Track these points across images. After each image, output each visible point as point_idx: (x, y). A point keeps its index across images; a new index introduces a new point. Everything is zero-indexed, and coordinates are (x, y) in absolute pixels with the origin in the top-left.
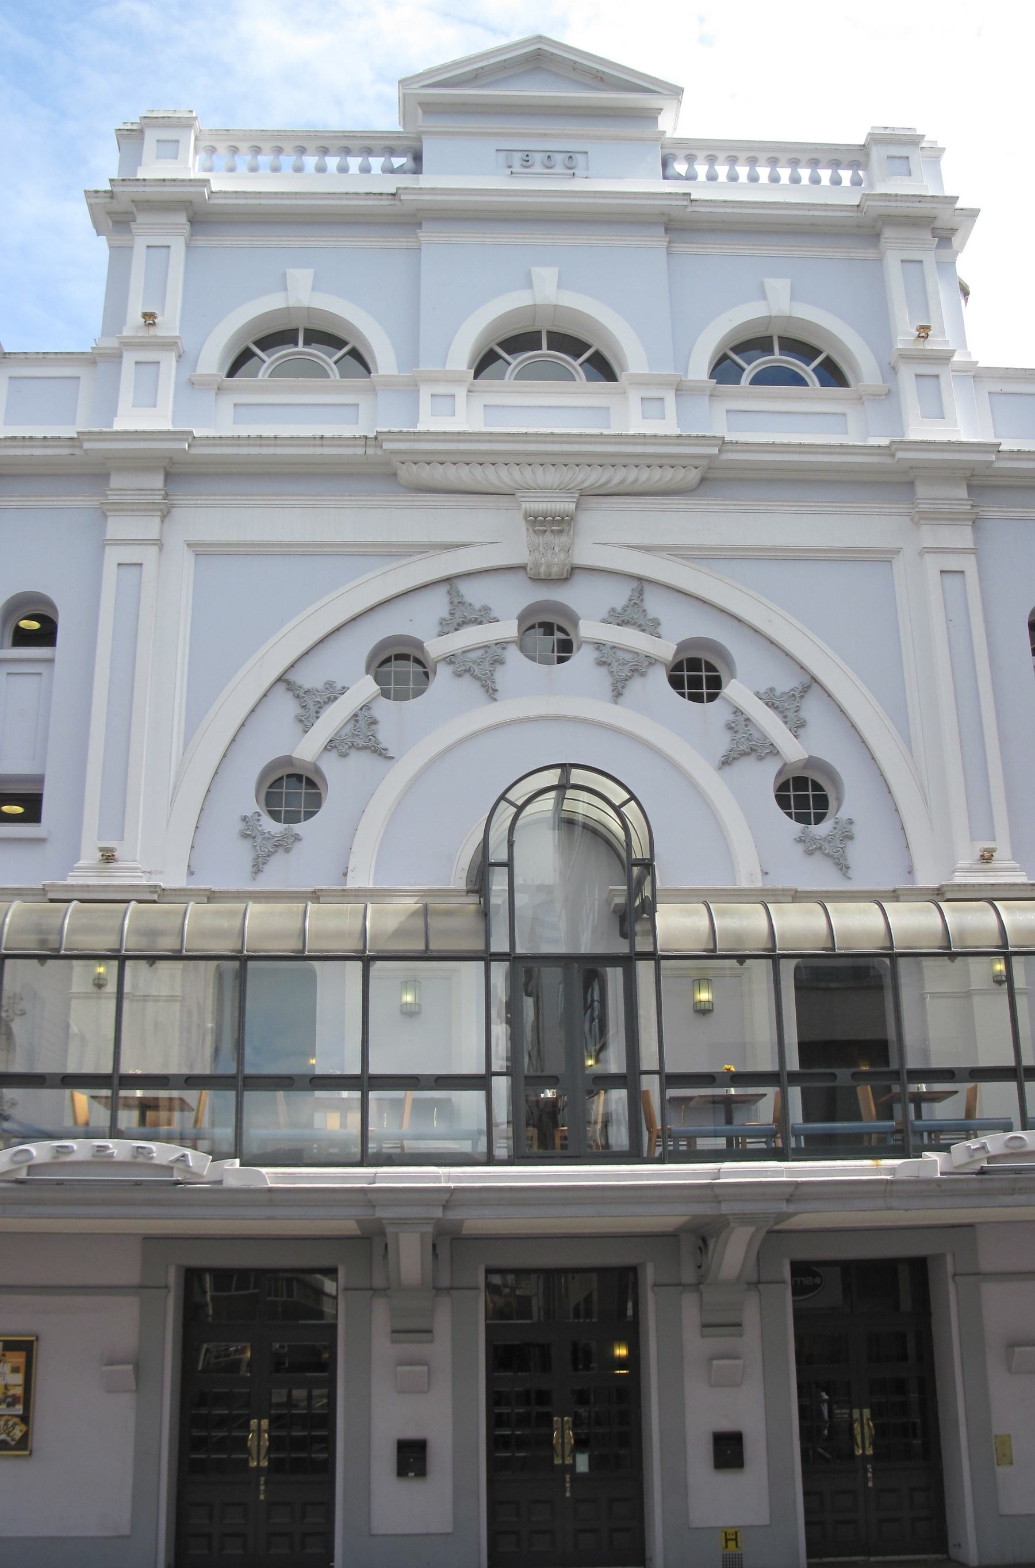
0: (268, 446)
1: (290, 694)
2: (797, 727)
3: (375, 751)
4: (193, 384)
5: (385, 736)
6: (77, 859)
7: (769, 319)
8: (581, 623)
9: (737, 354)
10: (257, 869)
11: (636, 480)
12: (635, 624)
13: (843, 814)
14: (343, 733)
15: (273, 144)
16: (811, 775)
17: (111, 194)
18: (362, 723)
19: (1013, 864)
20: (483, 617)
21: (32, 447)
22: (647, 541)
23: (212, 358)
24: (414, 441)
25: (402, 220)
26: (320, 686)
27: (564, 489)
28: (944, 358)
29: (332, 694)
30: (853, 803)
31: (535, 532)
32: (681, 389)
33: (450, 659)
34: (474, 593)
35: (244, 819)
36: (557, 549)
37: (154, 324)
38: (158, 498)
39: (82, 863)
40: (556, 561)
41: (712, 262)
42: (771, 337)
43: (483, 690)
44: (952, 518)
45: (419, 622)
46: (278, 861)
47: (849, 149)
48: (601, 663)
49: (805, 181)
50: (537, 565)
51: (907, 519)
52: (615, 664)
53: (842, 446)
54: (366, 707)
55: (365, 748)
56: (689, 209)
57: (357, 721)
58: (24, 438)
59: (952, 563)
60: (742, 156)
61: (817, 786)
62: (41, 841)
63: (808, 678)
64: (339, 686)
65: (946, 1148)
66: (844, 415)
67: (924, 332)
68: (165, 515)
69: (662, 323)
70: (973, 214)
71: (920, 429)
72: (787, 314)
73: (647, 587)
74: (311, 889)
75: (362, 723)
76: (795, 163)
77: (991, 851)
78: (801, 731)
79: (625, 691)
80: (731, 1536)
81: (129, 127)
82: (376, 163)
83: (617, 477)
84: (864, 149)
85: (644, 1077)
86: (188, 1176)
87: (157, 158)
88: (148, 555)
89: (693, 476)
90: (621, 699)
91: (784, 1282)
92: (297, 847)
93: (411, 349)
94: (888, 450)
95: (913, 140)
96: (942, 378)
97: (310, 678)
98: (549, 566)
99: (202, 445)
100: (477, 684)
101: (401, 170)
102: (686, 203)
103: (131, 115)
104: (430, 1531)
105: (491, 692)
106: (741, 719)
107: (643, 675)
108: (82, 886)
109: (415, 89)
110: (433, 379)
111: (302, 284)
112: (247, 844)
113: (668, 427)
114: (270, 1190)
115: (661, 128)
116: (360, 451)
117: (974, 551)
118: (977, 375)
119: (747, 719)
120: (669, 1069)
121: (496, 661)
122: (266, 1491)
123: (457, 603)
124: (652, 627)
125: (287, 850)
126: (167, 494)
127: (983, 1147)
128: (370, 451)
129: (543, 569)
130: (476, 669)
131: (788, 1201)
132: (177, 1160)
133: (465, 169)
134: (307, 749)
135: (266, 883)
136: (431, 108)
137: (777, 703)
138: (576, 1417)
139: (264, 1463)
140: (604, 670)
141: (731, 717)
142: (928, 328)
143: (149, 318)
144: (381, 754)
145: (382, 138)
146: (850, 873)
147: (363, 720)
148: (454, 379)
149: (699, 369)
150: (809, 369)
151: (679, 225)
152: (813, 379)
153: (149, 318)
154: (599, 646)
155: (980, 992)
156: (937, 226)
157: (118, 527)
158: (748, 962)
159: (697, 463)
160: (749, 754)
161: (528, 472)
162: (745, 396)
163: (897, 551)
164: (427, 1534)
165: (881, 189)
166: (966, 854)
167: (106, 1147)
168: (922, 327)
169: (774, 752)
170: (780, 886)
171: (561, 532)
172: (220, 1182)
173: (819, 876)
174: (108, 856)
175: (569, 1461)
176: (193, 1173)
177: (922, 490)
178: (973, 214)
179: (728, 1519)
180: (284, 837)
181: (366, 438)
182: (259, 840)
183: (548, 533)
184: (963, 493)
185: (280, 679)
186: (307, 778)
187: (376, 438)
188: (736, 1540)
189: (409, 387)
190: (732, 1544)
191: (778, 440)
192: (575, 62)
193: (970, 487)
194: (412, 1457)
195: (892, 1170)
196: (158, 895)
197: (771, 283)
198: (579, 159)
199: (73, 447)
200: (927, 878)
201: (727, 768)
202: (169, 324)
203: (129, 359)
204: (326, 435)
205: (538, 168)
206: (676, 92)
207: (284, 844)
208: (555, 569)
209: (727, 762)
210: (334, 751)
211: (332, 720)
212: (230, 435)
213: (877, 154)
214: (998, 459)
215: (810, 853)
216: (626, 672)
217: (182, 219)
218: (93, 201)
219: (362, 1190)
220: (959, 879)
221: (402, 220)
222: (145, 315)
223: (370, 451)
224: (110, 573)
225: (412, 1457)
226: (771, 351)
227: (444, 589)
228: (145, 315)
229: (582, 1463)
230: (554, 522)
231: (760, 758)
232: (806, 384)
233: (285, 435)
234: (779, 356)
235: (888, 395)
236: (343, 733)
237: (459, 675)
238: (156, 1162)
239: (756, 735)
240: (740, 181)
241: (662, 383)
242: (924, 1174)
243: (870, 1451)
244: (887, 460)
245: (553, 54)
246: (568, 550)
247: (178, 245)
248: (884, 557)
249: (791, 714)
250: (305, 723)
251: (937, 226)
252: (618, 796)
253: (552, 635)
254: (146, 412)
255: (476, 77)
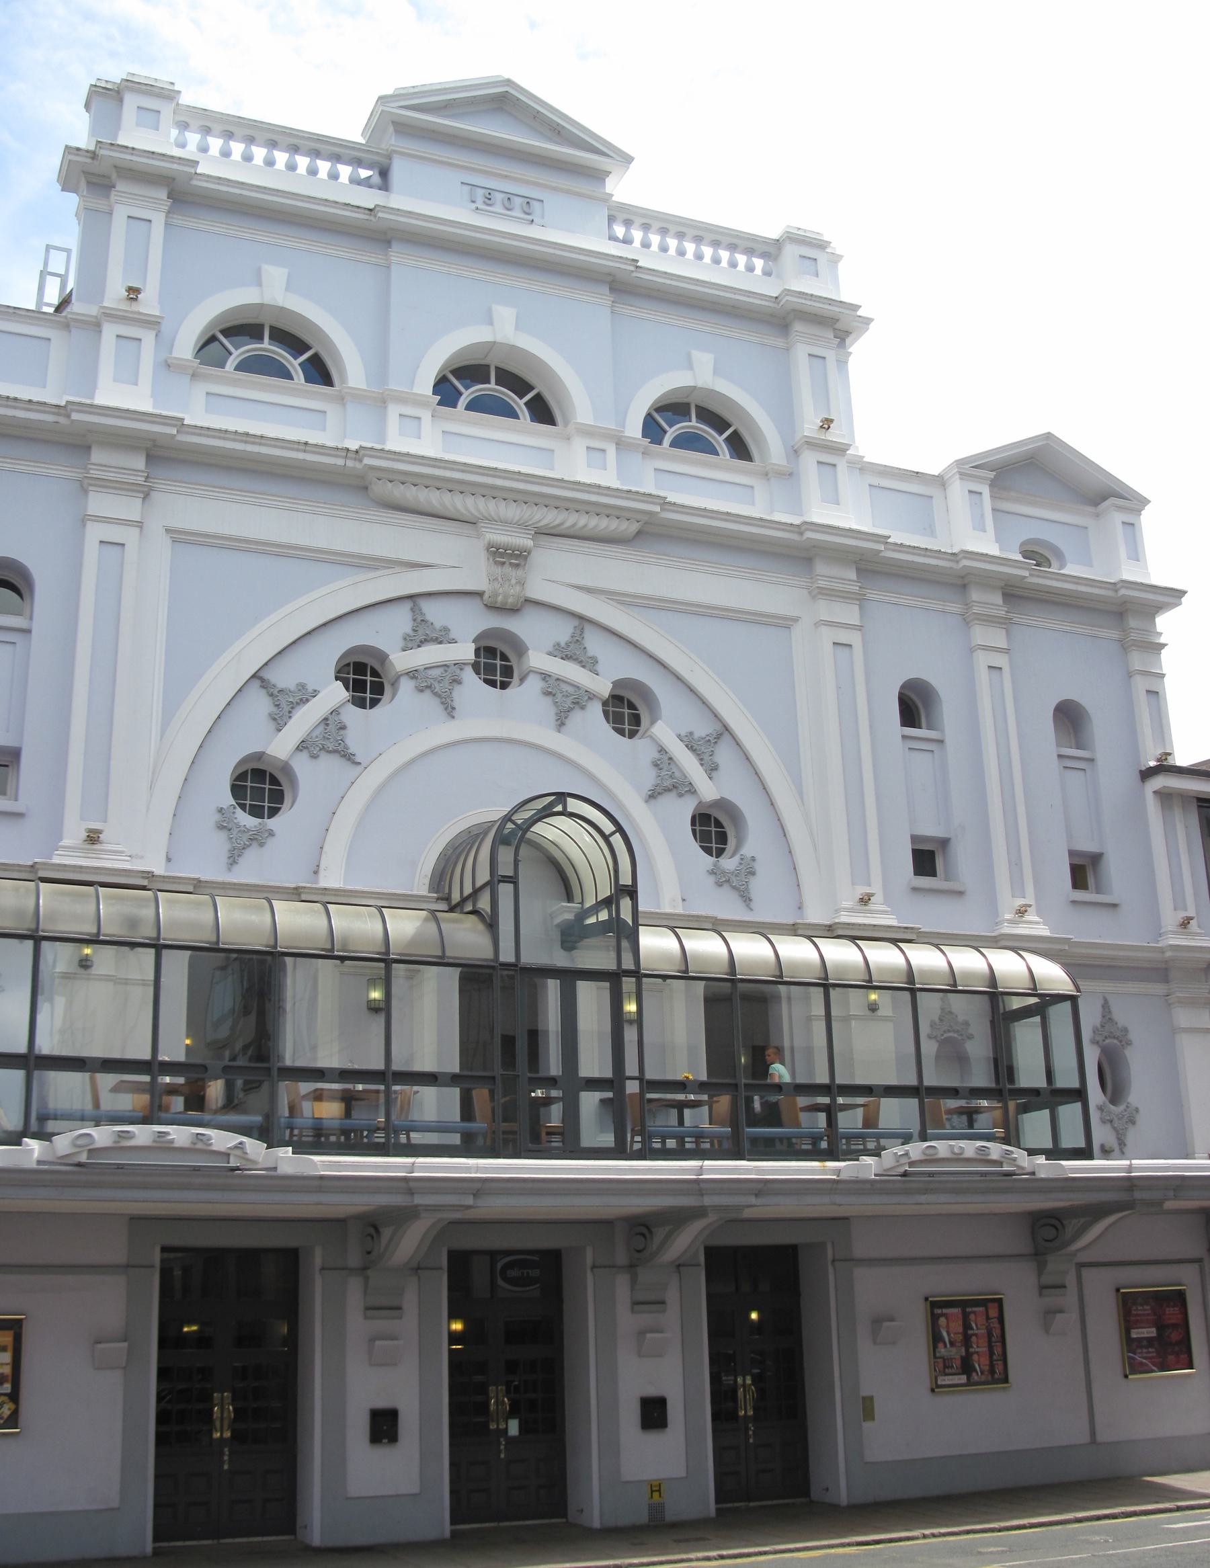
0: (253, 443)
1: (264, 691)
2: (712, 769)
3: (344, 756)
4: (169, 365)
5: (353, 742)
6: (61, 839)
7: (694, 388)
8: (530, 652)
9: (457, 378)
10: (233, 859)
11: (585, 526)
12: (576, 660)
13: (748, 850)
14: (314, 735)
15: (202, 123)
16: (716, 813)
17: (93, 155)
18: (332, 728)
19: (1036, 919)
20: (442, 637)
21: (15, 408)
22: (590, 584)
23: (185, 345)
24: (393, 460)
25: (377, 235)
26: (292, 687)
27: (522, 525)
28: (840, 450)
29: (304, 696)
30: (755, 842)
31: (496, 563)
32: (622, 444)
33: (413, 674)
34: (435, 612)
35: (221, 810)
36: (513, 581)
37: (136, 299)
38: (140, 480)
39: (66, 842)
40: (510, 593)
41: (653, 329)
42: (488, 366)
43: (442, 707)
44: (845, 596)
45: (385, 635)
46: (252, 855)
47: (765, 241)
48: (548, 693)
49: (741, 267)
50: (496, 594)
51: (806, 592)
52: (559, 696)
53: (761, 519)
54: (335, 712)
55: (335, 751)
56: (634, 274)
57: (327, 725)
58: (8, 398)
59: (844, 636)
60: (656, 225)
61: (718, 824)
62: (20, 815)
63: (719, 727)
64: (310, 688)
65: (876, 1153)
66: (752, 487)
67: (827, 424)
68: (146, 497)
69: (605, 374)
70: (868, 321)
71: (821, 514)
72: (281, 304)
73: (588, 629)
74: (293, 885)
75: (332, 728)
76: (229, 135)
77: (870, 896)
78: (714, 774)
79: (567, 721)
80: (656, 1488)
81: (103, 85)
82: (345, 171)
83: (571, 520)
84: (778, 244)
85: (628, 1082)
86: (244, 1162)
87: (138, 125)
88: (128, 536)
89: (634, 527)
90: (563, 729)
91: (699, 1265)
92: (271, 842)
93: (380, 364)
94: (799, 529)
95: (822, 245)
96: (839, 468)
97: (284, 678)
98: (506, 597)
99: (188, 433)
100: (437, 701)
101: (366, 183)
102: (632, 268)
103: (114, 73)
104: (400, 1492)
105: (450, 710)
106: (665, 758)
107: (583, 708)
108: (74, 866)
109: (392, 108)
110: (402, 399)
111: (278, 282)
112: (223, 835)
113: (609, 478)
114: (322, 1178)
115: (608, 190)
116: (340, 462)
117: (859, 628)
118: (863, 467)
119: (670, 759)
120: (649, 1075)
121: (454, 681)
122: (230, 1461)
123: (420, 621)
124: (591, 664)
125: (262, 845)
126: (147, 477)
127: (906, 1154)
128: (350, 463)
129: (500, 598)
130: (437, 685)
131: (756, 1195)
132: (236, 1147)
133: (429, 195)
134: (281, 747)
135: (244, 874)
136: (403, 128)
137: (696, 747)
138: (508, 1384)
139: (227, 1434)
140: (549, 700)
141: (656, 755)
142: (832, 421)
143: (133, 293)
144: (349, 759)
145: (354, 148)
146: (753, 905)
147: (331, 723)
148: (417, 401)
149: (634, 429)
150: (296, 363)
151: (624, 286)
152: (524, 413)
153: (133, 293)
154: (545, 676)
155: (856, 1017)
156: (835, 325)
157: (99, 503)
158: (669, 981)
159: (639, 517)
160: (670, 790)
161: (492, 504)
162: (461, 421)
163: (796, 620)
164: (397, 1496)
165: (796, 286)
166: (847, 897)
167: (167, 1133)
168: (827, 420)
169: (692, 791)
170: (704, 914)
171: (517, 565)
172: (275, 1169)
173: (726, 906)
174: (93, 838)
175: (502, 1426)
176: (248, 1160)
177: (821, 568)
178: (868, 321)
179: (651, 1473)
180: (259, 832)
181: (348, 450)
182: (235, 831)
183: (507, 565)
184: (853, 575)
185: (254, 676)
186: (271, 775)
187: (357, 452)
188: (659, 1491)
189: (380, 401)
190: (656, 1495)
191: (709, 507)
192: (538, 112)
193: (1004, 595)
194: (654, 1413)
195: (838, 1171)
196: (146, 883)
197: (696, 354)
198: (535, 204)
199: (59, 414)
200: (815, 915)
201: (653, 802)
202: (149, 304)
203: (110, 331)
204: (311, 441)
205: (498, 208)
206: (628, 159)
207: (258, 839)
208: (510, 600)
209: (653, 796)
210: (305, 751)
211: (304, 721)
212: (217, 427)
213: (790, 252)
214: (1031, 575)
215: (719, 884)
216: (568, 704)
217: (163, 194)
218: (71, 157)
219: (405, 1179)
220: (845, 918)
221: (377, 235)
222: (130, 290)
223: (350, 463)
224: (91, 551)
225: (384, 1426)
226: (260, 338)
227: (408, 605)
228: (130, 290)
229: (513, 1427)
230: (512, 556)
231: (680, 795)
232: (290, 377)
233: (271, 435)
234: (695, 423)
235: (789, 476)
236: (314, 735)
237: (421, 690)
238: (214, 1148)
239: (677, 774)
240: (276, 167)
241: (607, 435)
242: (863, 1175)
243: (751, 1413)
244: (795, 537)
245: (518, 99)
246: (522, 583)
247: (159, 219)
248: (785, 623)
249: (706, 757)
250: (279, 721)
251: (835, 325)
252: (608, 827)
253: (497, 663)
254: (126, 388)
255: (445, 107)
